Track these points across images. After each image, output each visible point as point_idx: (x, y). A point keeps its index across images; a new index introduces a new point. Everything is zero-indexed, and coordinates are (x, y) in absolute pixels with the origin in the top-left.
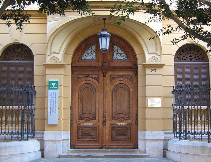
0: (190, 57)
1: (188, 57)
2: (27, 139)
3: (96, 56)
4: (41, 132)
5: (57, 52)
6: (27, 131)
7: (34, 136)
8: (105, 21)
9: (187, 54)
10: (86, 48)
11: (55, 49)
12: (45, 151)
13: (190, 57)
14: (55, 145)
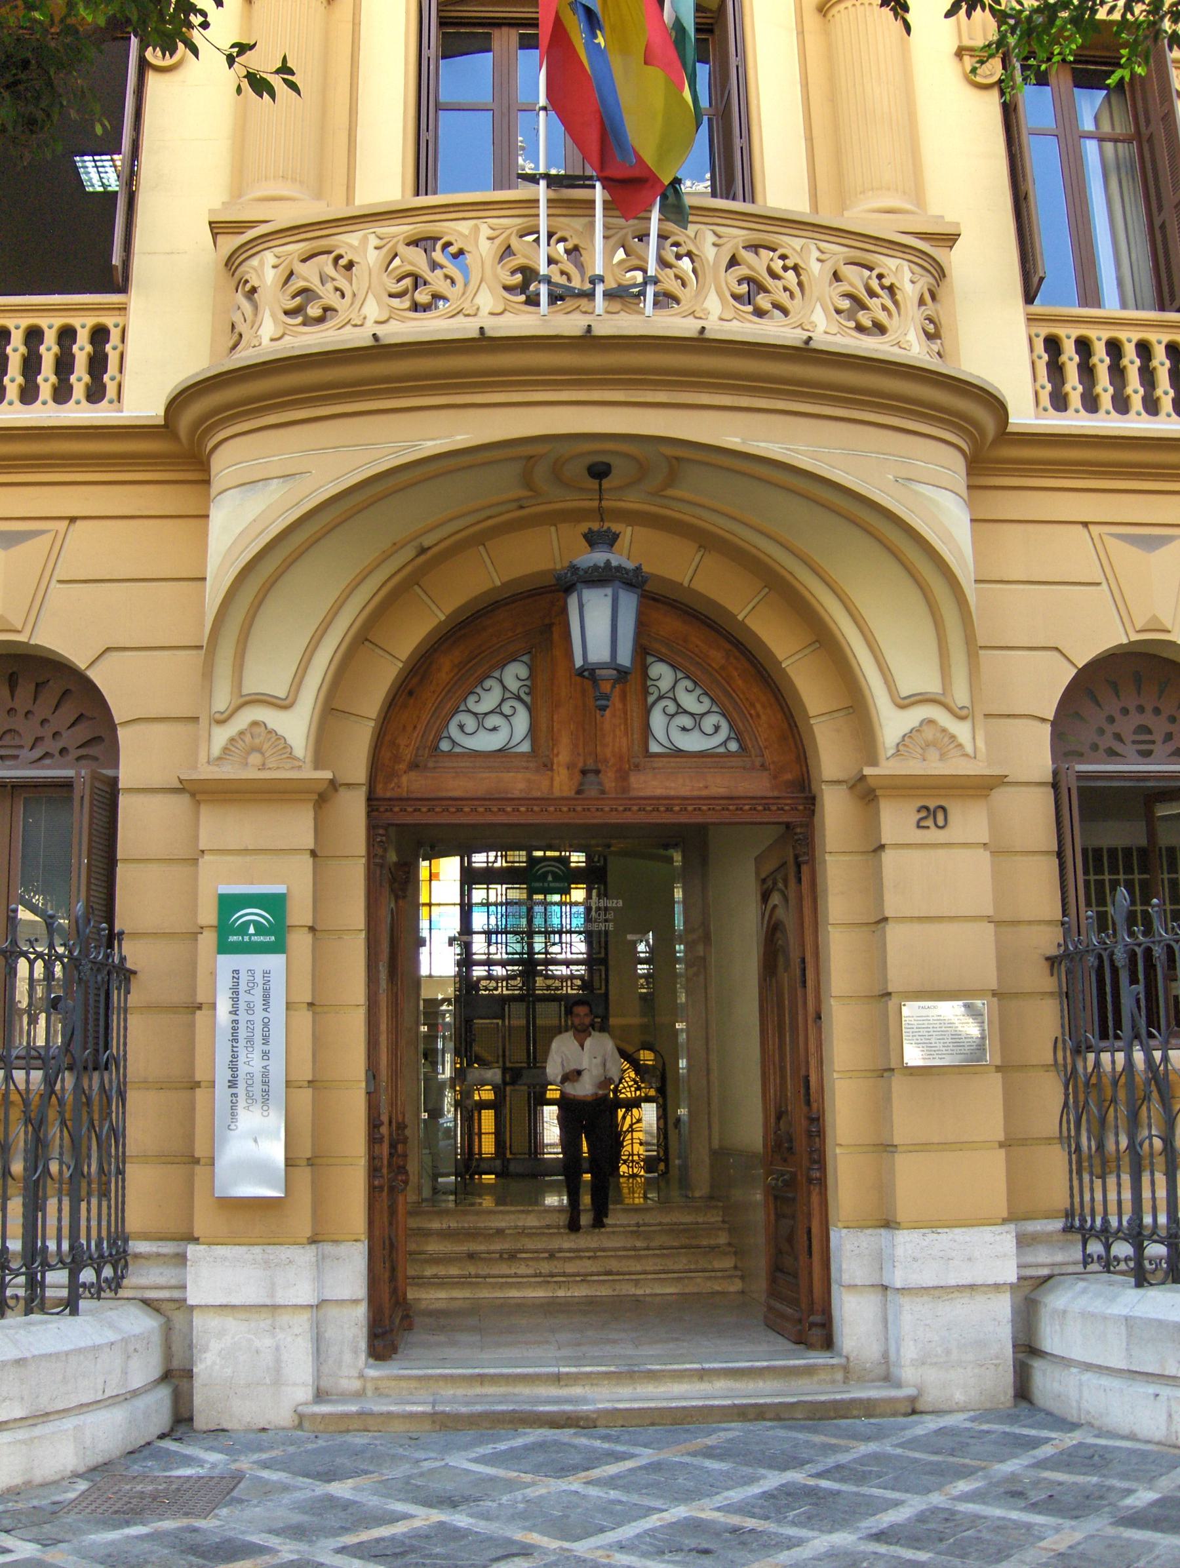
0: (1135, 732)
1: (1129, 737)
2: (71, 1305)
3: (533, 731)
4: (168, 1248)
5: (280, 691)
6: (65, 1246)
7: (123, 1277)
8: (606, 483)
9: (1118, 716)
10: (471, 677)
11: (269, 672)
12: (197, 1383)
13: (1135, 732)
14: (266, 1342)
